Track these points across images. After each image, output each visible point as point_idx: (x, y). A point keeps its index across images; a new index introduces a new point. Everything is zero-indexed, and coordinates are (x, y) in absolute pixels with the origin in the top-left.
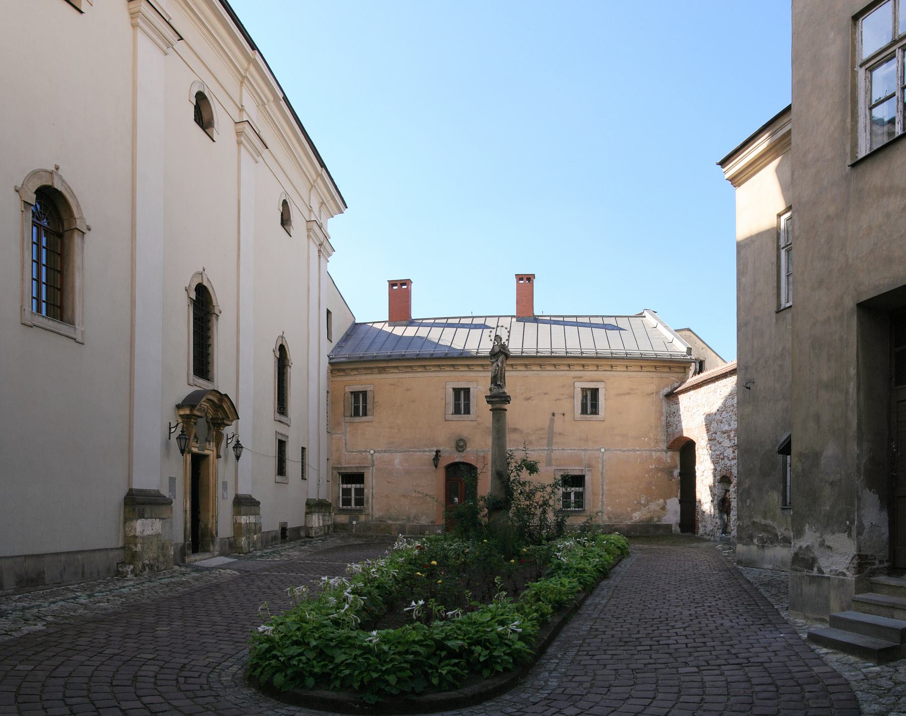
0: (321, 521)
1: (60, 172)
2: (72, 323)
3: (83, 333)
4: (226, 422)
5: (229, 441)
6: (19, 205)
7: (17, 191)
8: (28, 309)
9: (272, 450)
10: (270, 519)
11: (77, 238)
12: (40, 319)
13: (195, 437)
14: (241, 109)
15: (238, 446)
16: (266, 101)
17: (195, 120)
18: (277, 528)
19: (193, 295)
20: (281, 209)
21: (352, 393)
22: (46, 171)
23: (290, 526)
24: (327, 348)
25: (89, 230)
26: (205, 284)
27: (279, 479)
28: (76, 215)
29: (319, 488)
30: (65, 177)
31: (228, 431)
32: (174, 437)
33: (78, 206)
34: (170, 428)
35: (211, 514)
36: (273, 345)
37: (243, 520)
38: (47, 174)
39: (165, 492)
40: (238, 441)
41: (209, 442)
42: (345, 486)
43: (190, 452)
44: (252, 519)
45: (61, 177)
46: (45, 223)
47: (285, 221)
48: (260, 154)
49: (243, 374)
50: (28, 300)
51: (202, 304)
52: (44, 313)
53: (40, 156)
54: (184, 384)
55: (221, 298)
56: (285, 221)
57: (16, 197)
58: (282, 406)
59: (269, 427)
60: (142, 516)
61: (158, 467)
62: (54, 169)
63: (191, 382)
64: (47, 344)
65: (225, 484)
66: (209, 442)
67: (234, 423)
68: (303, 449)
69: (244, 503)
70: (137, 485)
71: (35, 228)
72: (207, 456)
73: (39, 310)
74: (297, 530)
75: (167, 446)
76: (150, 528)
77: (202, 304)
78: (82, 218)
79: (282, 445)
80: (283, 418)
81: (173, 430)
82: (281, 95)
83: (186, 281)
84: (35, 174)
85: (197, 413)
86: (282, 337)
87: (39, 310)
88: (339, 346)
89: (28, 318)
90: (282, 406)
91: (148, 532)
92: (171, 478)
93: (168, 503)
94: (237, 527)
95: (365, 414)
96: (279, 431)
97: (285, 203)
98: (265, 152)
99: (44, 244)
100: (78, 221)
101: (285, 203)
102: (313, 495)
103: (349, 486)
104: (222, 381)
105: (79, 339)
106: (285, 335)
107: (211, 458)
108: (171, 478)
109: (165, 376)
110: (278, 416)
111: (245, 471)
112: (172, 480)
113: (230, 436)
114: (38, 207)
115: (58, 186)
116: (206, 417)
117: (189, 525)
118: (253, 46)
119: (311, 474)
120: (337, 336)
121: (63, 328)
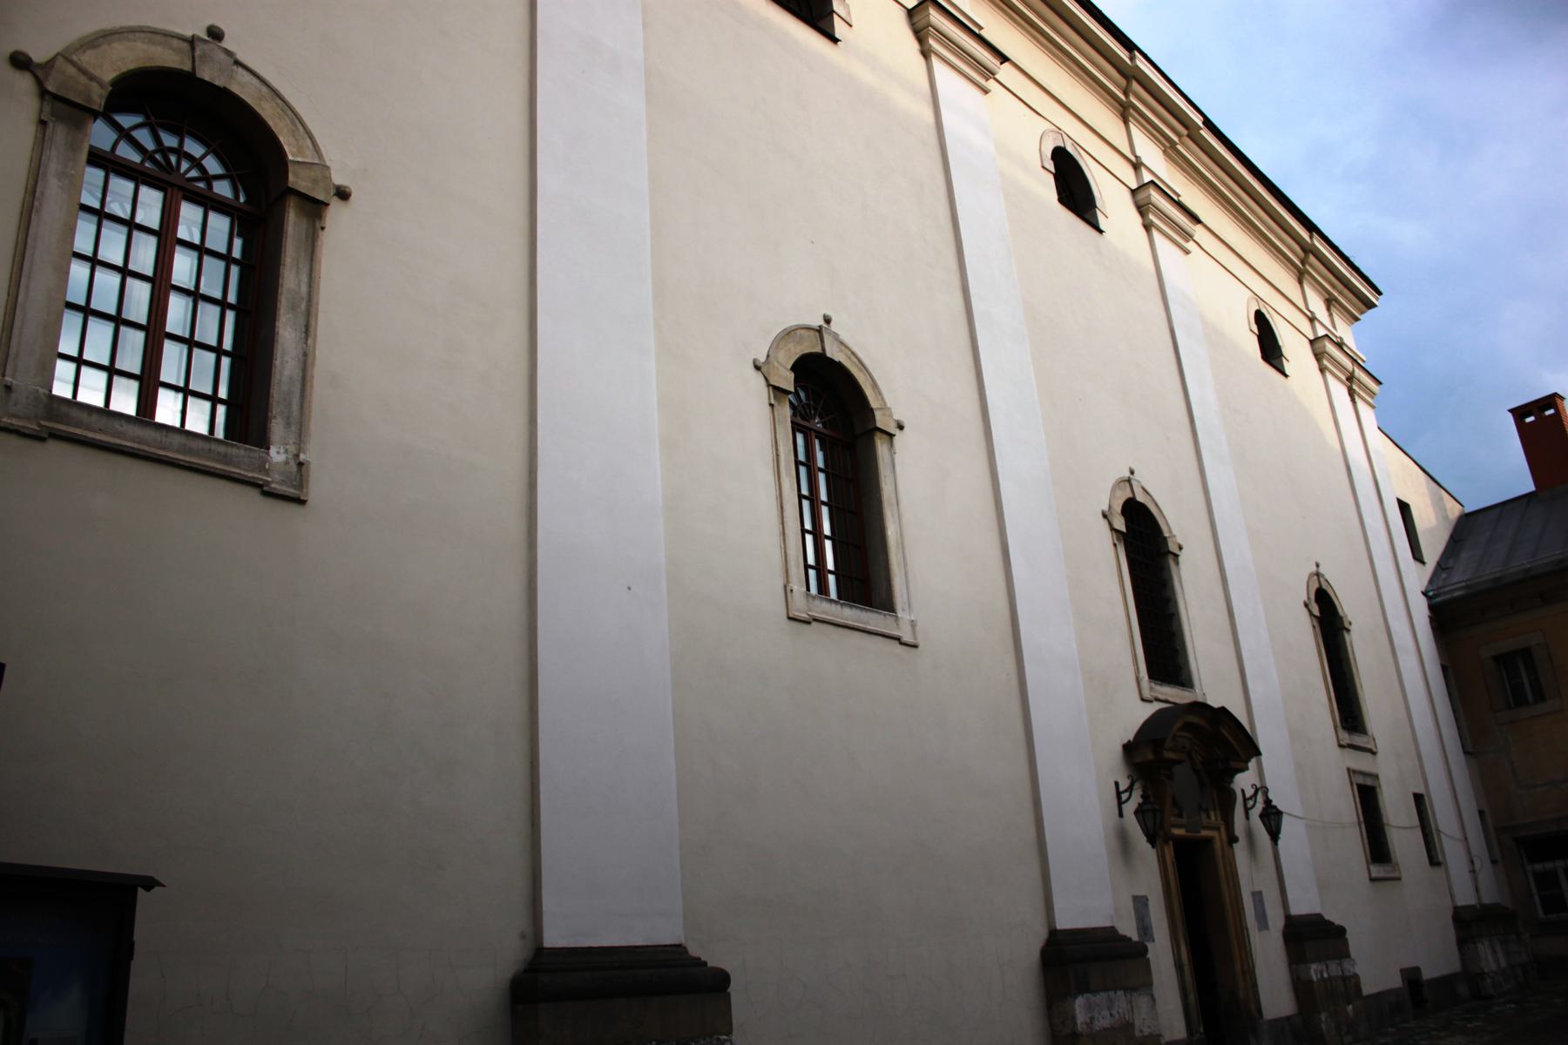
0: (1500, 955)
1: (834, 327)
2: (888, 606)
3: (913, 624)
4: (1233, 764)
5: (1251, 803)
6: (761, 393)
7: (758, 368)
8: (798, 587)
9: (1346, 807)
10: (1375, 967)
11: (881, 447)
12: (825, 606)
13: (1175, 803)
14: (1137, 166)
15: (1272, 817)
16: (1175, 139)
17: (1061, 201)
18: (1396, 982)
19: (1120, 524)
20: (1255, 328)
21: (1497, 659)
22: (809, 328)
23: (1427, 974)
24: (1417, 578)
25: (901, 427)
26: (1140, 498)
27: (1377, 871)
28: (874, 404)
29: (1475, 880)
30: (844, 337)
31: (1244, 782)
32: (1130, 808)
33: (875, 385)
34: (1119, 794)
35: (1238, 967)
36: (1301, 592)
37: (1315, 971)
38: (812, 333)
39: (1128, 929)
40: (1268, 802)
41: (1207, 811)
42: (1539, 867)
43: (1168, 838)
44: (1334, 969)
45: (836, 337)
46: (817, 424)
47: (1271, 350)
48: (1188, 236)
49: (1251, 660)
50: (797, 571)
51: (1143, 539)
52: (833, 594)
53: (795, 295)
54: (1131, 710)
55: (1179, 521)
56: (1271, 350)
57: (757, 381)
58: (1349, 712)
59: (1333, 763)
60: (1084, 988)
61: (1101, 877)
62: (822, 323)
63: (1147, 694)
64: (844, 656)
65: (1258, 897)
66: (1207, 811)
67: (1252, 764)
68: (1418, 798)
69: (1311, 937)
70: (1066, 920)
71: (800, 438)
72: (1209, 840)
73: (823, 588)
74: (1445, 982)
75: (1123, 839)
76: (1106, 1013)
77: (1143, 539)
78: (884, 408)
79: (1367, 795)
80: (1359, 740)
81: (1124, 797)
82: (1198, 120)
83: (1102, 497)
84: (789, 334)
85: (1169, 755)
86: (1318, 574)
87: (823, 588)
88: (1441, 566)
89: (800, 606)
90: (1349, 712)
91: (1103, 1021)
92: (1136, 899)
93: (1135, 953)
94: (1301, 987)
95: (1540, 697)
96: (1354, 766)
97: (1260, 318)
98: (1198, 232)
99: (820, 463)
100: (878, 415)
101: (1260, 318)
102: (1465, 897)
103: (1549, 865)
104: (1213, 683)
105: (907, 638)
106: (1321, 570)
107: (1218, 845)
108: (1136, 899)
109: (1090, 691)
110: (1346, 737)
111: (1300, 861)
112: (1140, 903)
113: (1249, 792)
114: (802, 395)
115: (833, 352)
116: (1187, 763)
117: (1192, 997)
118: (1129, 46)
119: (1452, 850)
120: (1433, 550)
121: (874, 619)
